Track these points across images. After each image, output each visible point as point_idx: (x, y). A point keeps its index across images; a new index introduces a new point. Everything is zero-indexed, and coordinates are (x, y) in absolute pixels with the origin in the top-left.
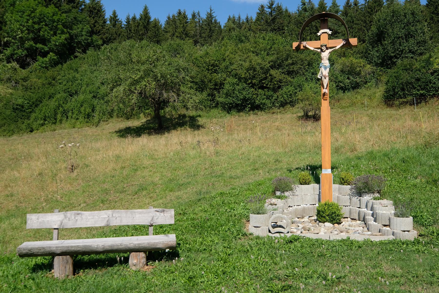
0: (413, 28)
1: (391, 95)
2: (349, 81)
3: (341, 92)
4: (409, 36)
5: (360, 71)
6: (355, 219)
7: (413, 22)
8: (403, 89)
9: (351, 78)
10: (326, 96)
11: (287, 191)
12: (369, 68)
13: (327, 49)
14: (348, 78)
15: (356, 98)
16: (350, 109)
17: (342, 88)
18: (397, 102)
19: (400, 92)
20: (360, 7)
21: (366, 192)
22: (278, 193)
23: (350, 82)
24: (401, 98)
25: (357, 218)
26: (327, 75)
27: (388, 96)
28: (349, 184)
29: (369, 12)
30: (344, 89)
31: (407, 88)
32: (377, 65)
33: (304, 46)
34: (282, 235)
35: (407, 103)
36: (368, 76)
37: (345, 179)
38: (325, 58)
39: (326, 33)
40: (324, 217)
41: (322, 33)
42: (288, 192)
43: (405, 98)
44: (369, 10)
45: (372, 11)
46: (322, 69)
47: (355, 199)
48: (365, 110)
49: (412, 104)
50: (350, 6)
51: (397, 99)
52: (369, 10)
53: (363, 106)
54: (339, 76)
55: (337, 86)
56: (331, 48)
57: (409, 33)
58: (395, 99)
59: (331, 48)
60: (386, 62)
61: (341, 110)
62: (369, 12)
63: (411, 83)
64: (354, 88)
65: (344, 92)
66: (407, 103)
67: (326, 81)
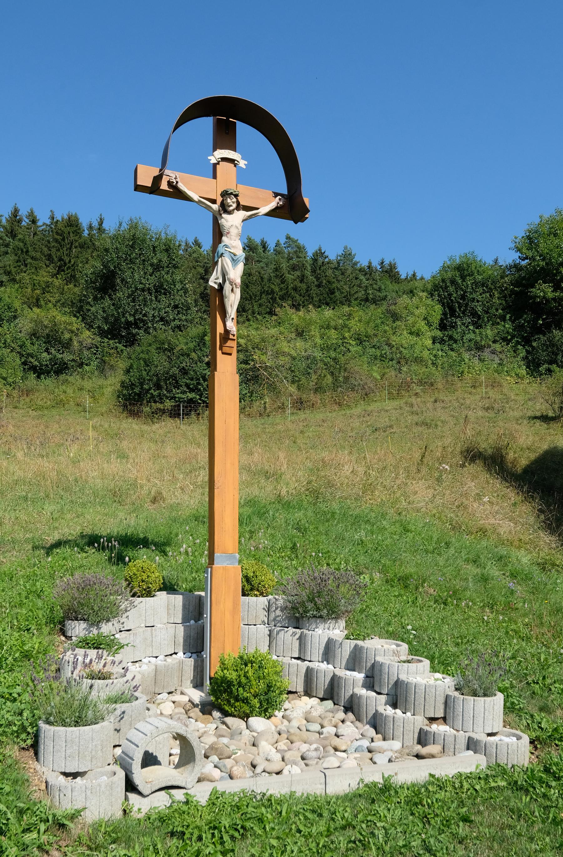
0: (168, 277)
1: (136, 394)
2: (48, 357)
3: (33, 376)
4: (160, 290)
5: (71, 339)
6: (296, 692)
7: (167, 267)
8: (158, 386)
9: (53, 351)
10: (229, 343)
11: (108, 620)
12: (87, 336)
13: (239, 207)
14: (47, 350)
15: (65, 392)
16: (54, 412)
17: (33, 369)
18: (147, 409)
19: (152, 391)
20: (41, 229)
21: (321, 617)
22: (78, 629)
23: (50, 359)
24: (155, 402)
25: (300, 688)
26: (238, 281)
27: (130, 395)
28: (262, 594)
29: (56, 241)
30: (40, 372)
31: (166, 384)
32: (102, 333)
33: (170, 184)
34: (179, 795)
35: (163, 411)
36: (86, 353)
37: (255, 582)
38: (234, 232)
39: (232, 161)
40: (246, 701)
41: (224, 159)
42: (110, 624)
43: (161, 403)
44: (59, 237)
45: (63, 240)
46: (227, 261)
47: (289, 637)
48: (85, 417)
49: (174, 414)
50: (20, 221)
51: (147, 402)
52: (59, 237)
53: (80, 409)
54: (28, 343)
55: (24, 363)
56: (247, 208)
57: (161, 286)
58: (145, 402)
59: (247, 208)
60: (120, 331)
61: (35, 413)
62: (56, 241)
63: (174, 377)
64: (58, 372)
65: (39, 377)
66: (163, 411)
67: (233, 300)
